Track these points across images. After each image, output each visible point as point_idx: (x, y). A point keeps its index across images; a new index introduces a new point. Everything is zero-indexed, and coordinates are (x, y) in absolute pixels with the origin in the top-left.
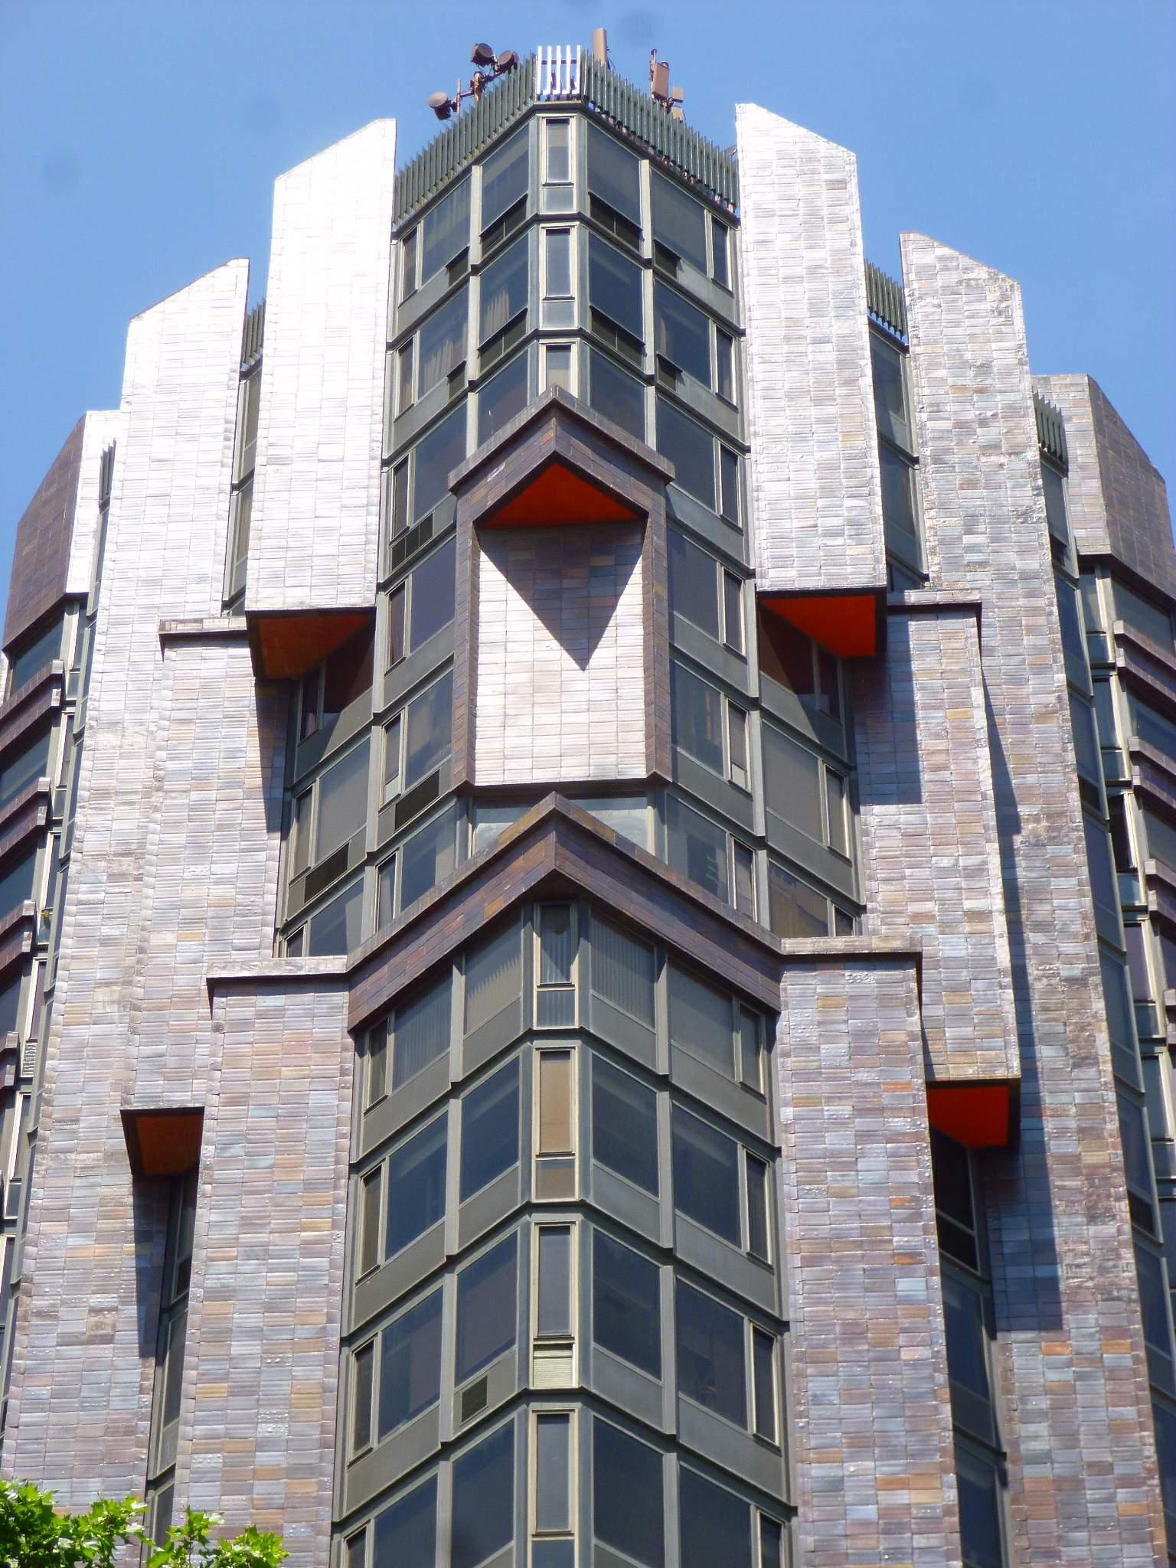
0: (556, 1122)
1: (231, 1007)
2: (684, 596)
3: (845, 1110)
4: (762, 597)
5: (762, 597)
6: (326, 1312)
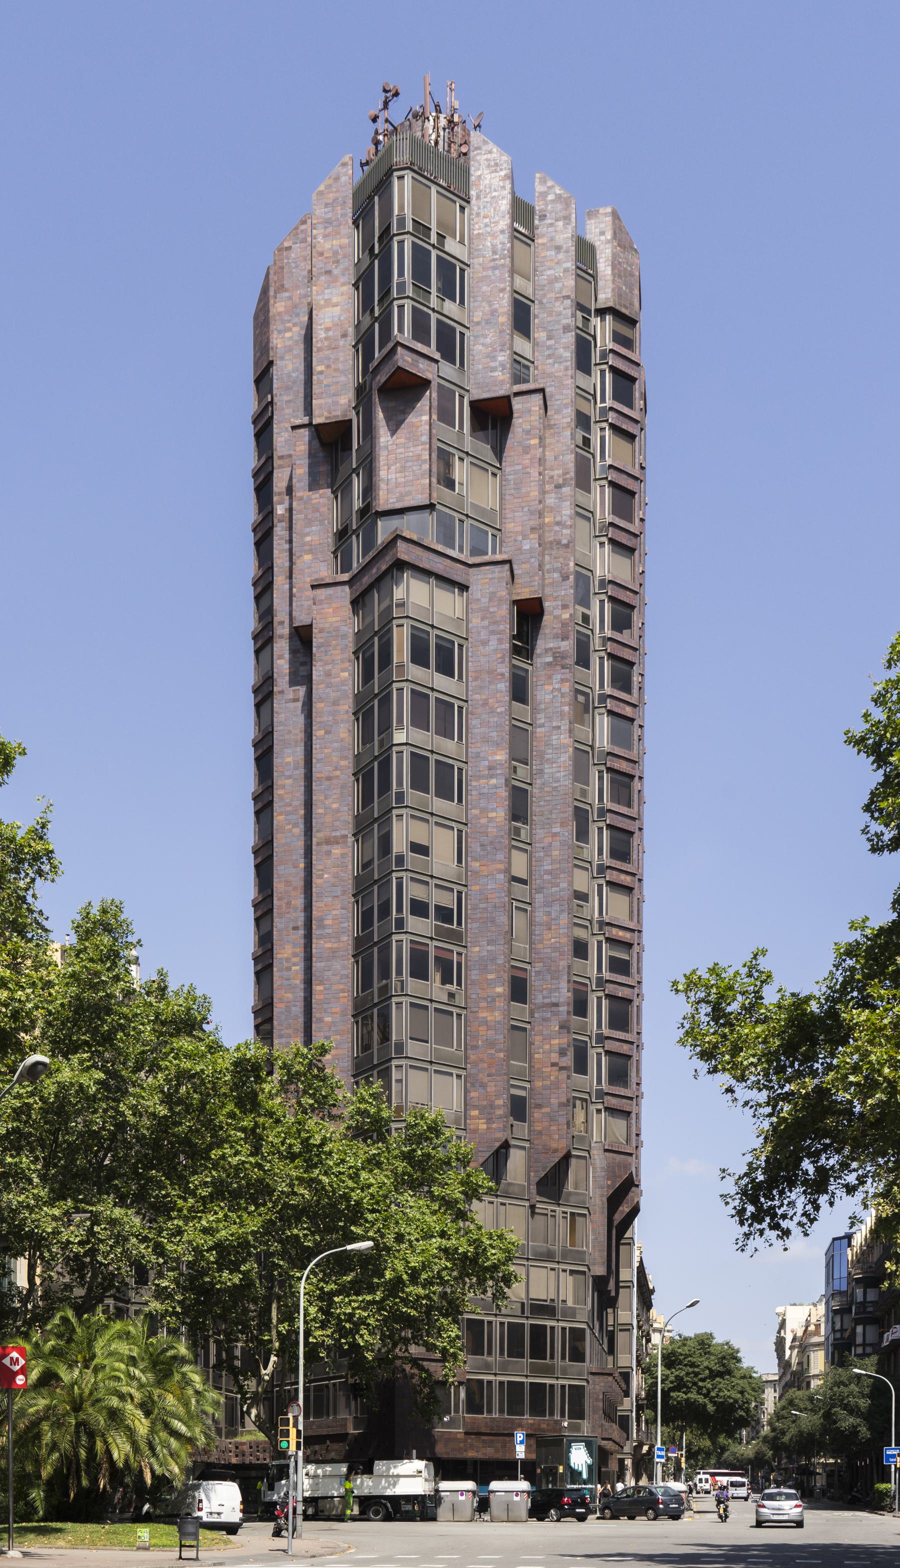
0: (400, 650)
1: (322, 593)
2: (446, 415)
3: (486, 623)
4: (474, 404)
5: (474, 404)
6: (348, 765)
